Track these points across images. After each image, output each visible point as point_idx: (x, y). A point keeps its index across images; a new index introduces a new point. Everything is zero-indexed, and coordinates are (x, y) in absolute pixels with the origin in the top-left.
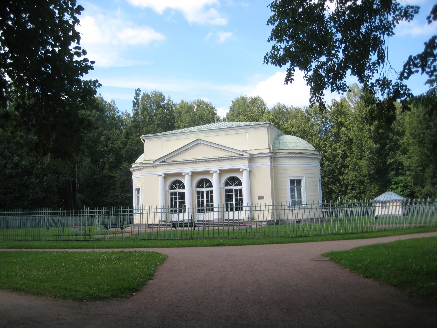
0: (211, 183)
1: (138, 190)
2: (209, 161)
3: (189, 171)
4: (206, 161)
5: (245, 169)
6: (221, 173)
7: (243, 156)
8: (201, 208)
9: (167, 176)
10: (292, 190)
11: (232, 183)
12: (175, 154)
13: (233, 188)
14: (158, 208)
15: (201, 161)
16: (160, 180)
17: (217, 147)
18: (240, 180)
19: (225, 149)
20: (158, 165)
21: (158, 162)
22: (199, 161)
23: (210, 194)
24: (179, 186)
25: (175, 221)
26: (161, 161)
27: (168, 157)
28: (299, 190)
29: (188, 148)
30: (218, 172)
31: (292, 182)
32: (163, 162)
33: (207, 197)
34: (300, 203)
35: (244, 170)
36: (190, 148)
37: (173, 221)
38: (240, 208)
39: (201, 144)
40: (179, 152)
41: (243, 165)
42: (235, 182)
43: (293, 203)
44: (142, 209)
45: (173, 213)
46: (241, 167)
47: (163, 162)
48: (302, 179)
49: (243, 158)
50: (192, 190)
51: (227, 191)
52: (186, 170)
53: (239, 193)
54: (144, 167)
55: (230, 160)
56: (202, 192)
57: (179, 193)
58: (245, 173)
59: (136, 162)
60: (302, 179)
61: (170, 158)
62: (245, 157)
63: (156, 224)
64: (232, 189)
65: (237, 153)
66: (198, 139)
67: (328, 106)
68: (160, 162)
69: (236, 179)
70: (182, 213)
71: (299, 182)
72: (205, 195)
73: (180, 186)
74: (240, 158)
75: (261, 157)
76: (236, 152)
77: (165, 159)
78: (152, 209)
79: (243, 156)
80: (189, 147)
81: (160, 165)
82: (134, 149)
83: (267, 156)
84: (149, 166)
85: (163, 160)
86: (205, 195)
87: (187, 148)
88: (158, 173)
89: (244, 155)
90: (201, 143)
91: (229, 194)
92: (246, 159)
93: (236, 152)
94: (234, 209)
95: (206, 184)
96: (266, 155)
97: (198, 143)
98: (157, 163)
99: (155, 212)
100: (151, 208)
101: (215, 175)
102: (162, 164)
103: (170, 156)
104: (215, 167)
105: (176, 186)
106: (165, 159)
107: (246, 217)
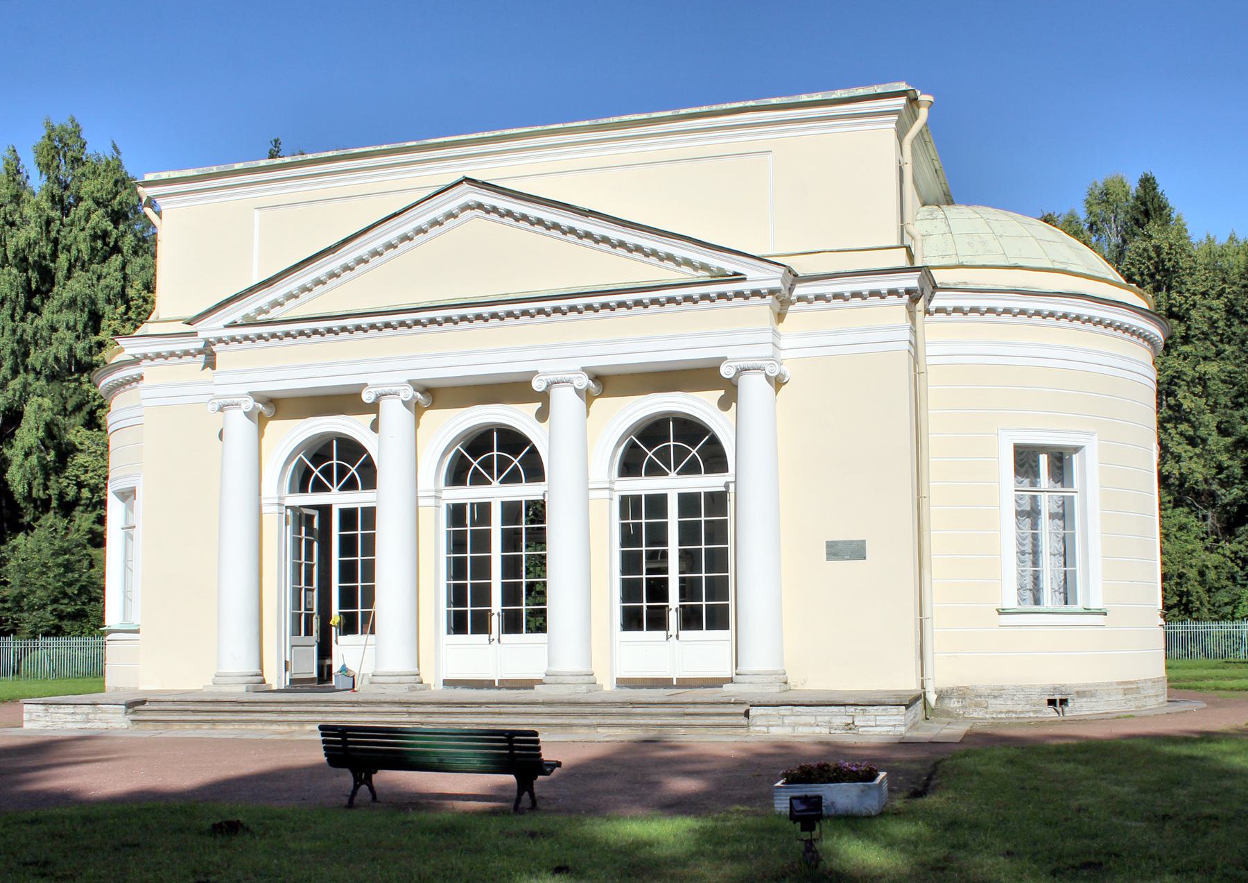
0: (714, 441)
13: (496, 493)
16: (239, 425)
31: (1025, 460)
34: (1067, 592)
42: (504, 463)
46: (370, 380)
49: (739, 294)
51: (629, 505)
56: (657, 504)
57: (503, 503)
62: (756, 293)
65: (688, 263)
66: (467, 179)
68: (234, 325)
69: (351, 448)
71: (1060, 461)
72: (673, 520)
73: (353, 470)
76: (698, 255)
86: (673, 520)
88: (219, 391)
93: (698, 255)
94: (496, 623)
95: (680, 453)
96: (883, 284)
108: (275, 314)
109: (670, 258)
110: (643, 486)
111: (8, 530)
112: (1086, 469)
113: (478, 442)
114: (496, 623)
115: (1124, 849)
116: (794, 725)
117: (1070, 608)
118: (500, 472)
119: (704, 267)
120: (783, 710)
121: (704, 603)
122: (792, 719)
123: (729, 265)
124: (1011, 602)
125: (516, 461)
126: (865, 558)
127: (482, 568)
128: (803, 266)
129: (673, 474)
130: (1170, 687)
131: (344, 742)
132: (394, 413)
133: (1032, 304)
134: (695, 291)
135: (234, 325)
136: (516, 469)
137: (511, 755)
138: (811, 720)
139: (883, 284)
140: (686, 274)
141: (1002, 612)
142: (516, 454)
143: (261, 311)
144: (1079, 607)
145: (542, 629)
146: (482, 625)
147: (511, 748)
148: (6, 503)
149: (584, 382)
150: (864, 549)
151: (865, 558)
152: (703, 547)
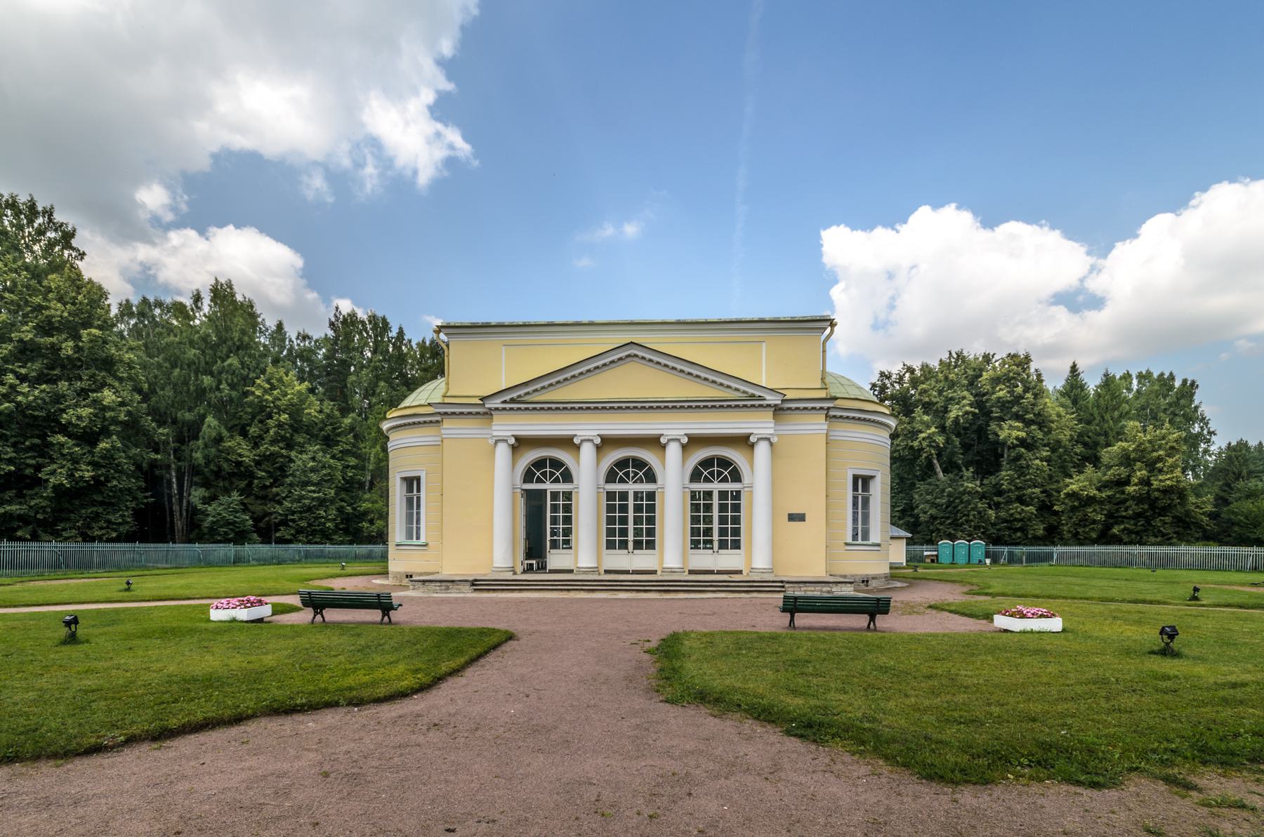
2: (628, 408)
3: (596, 433)
4: (690, 407)
5: (587, 438)
6: (517, 445)
7: (765, 399)
8: (714, 538)
9: (521, 444)
10: (855, 499)
12: (553, 381)
13: (631, 487)
15: (713, 407)
16: (503, 452)
17: (687, 369)
18: (567, 469)
19: (711, 377)
20: (497, 409)
21: (499, 401)
22: (581, 408)
24: (552, 474)
26: (508, 398)
27: (530, 389)
28: (866, 502)
29: (597, 368)
30: (598, 441)
31: (856, 478)
32: (512, 401)
34: (866, 536)
35: (672, 440)
38: (647, 541)
39: (636, 359)
40: (568, 375)
43: (855, 537)
46: (665, 432)
48: (872, 477)
49: (761, 406)
50: (514, 488)
51: (611, 496)
52: (587, 428)
53: (732, 503)
54: (446, 413)
55: (573, 412)
56: (624, 496)
59: (402, 405)
60: (872, 477)
61: (536, 394)
62: (769, 406)
64: (712, 492)
65: (737, 390)
68: (505, 402)
74: (753, 406)
75: (805, 409)
76: (742, 388)
77: (522, 392)
79: (765, 399)
80: (600, 363)
81: (504, 409)
83: (821, 408)
84: (462, 413)
85: (514, 395)
87: (584, 369)
88: (495, 433)
89: (767, 397)
90: (636, 356)
92: (768, 409)
94: (631, 545)
96: (818, 405)
97: (629, 356)
98: (496, 403)
101: (587, 451)
102: (511, 409)
103: (538, 386)
104: (674, 428)
105: (544, 474)
106: (522, 392)
108: (527, 398)
109: (729, 387)
110: (702, 487)
114: (631, 545)
116: (805, 591)
117: (415, 541)
119: (744, 392)
120: (801, 585)
121: (617, 538)
122: (805, 588)
123: (757, 393)
124: (850, 540)
128: (790, 395)
129: (548, 483)
131: (878, 604)
132: (587, 451)
133: (863, 416)
134: (741, 403)
135: (505, 402)
137: (379, 602)
138: (813, 589)
139: (818, 405)
140: (737, 395)
141: (847, 544)
143: (519, 396)
144: (870, 542)
145: (738, 547)
146: (624, 545)
147: (379, 599)
149: (512, 441)
152: (729, 514)
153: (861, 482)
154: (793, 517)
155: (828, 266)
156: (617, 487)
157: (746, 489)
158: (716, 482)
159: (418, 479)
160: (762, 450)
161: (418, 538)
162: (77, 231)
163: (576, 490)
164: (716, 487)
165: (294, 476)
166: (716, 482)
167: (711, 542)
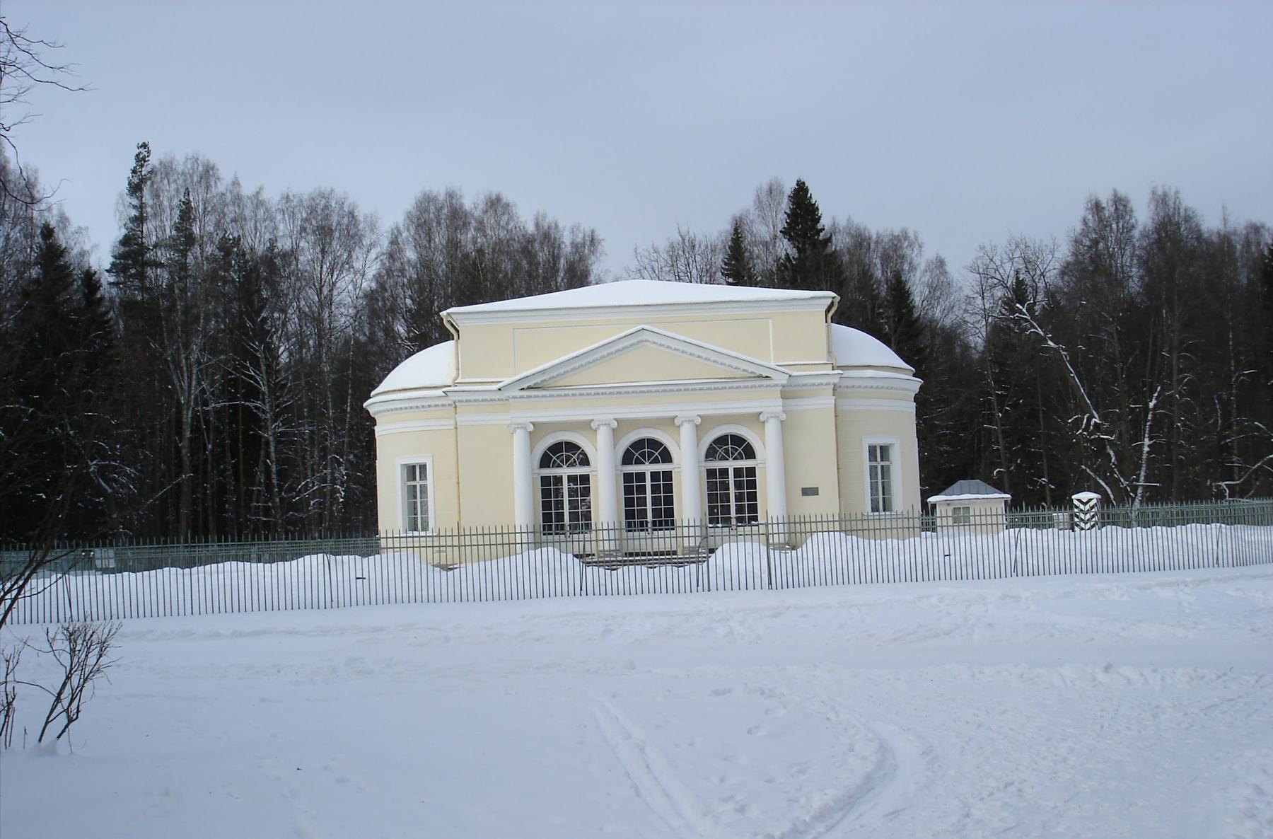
1: (414, 472)
8: (732, 516)
9: (538, 430)
10: (873, 470)
11: (727, 452)
13: (648, 468)
14: (474, 532)
16: (519, 442)
23: (664, 483)
25: (673, 551)
26: (525, 386)
31: (872, 450)
32: (530, 388)
33: (655, 489)
36: (629, 347)
37: (669, 551)
41: (771, 405)
42: (650, 454)
44: (767, 525)
45: (631, 531)
46: (594, 417)
47: (530, 388)
51: (711, 473)
53: (748, 479)
56: (641, 476)
57: (734, 469)
58: (772, 429)
62: (776, 385)
63: (664, 564)
67: (409, 261)
70: (635, 531)
71: (884, 450)
78: (502, 534)
80: (613, 350)
82: (369, 317)
85: (532, 383)
91: (662, 483)
94: (734, 522)
95: (568, 458)
99: (416, 544)
100: (505, 531)
107: (638, 540)
111: (199, 415)
112: (895, 456)
113: (556, 448)
114: (734, 522)
115: (940, 298)
118: (733, 454)
125: (657, 454)
126: (818, 494)
127: (656, 501)
129: (565, 466)
130: (1262, 525)
136: (740, 453)
142: (657, 451)
148: (1235, 363)
149: (615, 424)
150: (818, 491)
151: (818, 494)
153: (880, 453)
154: (807, 492)
155: (840, 243)
156: (634, 469)
157: (676, 470)
158: (565, 466)
159: (423, 467)
160: (772, 429)
161: (425, 529)
162: (264, 190)
163: (593, 473)
164: (731, 465)
165: (225, 479)
166: (731, 459)
167: (563, 526)
